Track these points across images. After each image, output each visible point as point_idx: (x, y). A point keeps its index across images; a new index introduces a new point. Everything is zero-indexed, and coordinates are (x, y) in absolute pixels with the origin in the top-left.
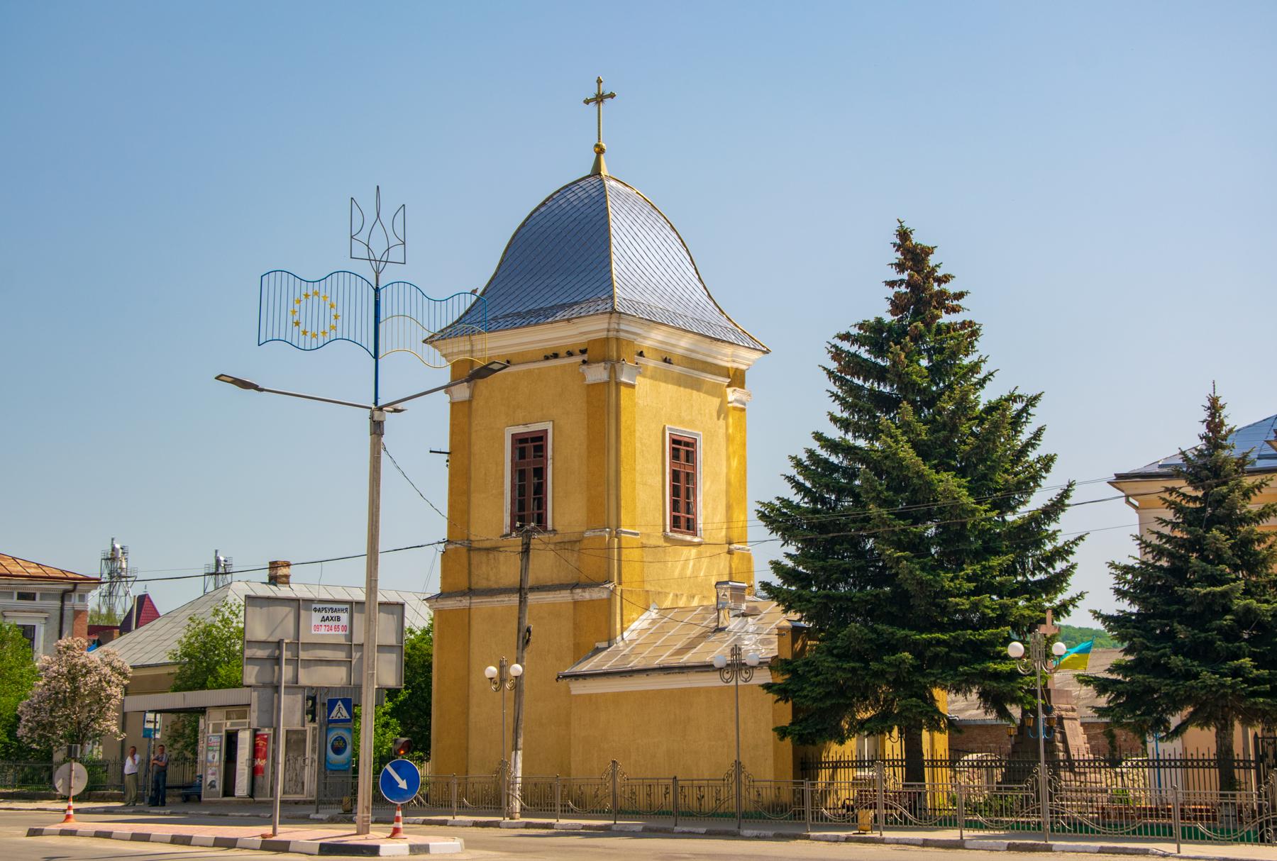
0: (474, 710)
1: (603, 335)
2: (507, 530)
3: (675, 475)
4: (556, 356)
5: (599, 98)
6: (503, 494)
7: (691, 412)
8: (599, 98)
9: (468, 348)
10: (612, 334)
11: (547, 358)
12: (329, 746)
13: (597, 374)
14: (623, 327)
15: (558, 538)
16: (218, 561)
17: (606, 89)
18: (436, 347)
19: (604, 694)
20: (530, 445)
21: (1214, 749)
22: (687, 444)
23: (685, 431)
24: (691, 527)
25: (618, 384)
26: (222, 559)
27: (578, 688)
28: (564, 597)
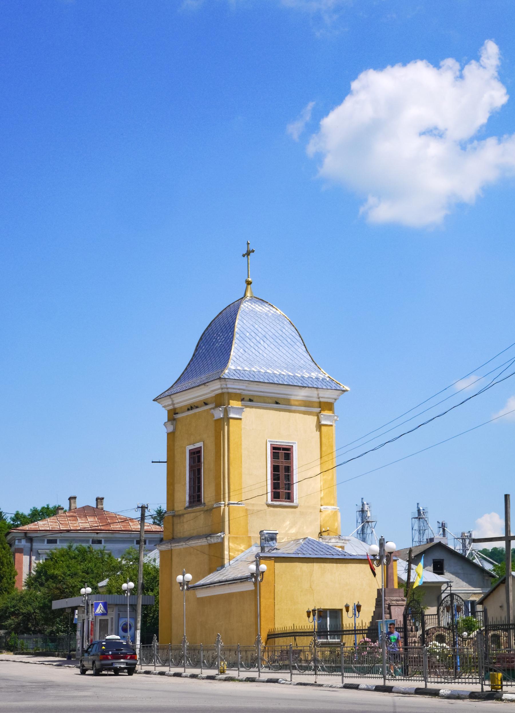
0: (174, 607)
1: (220, 391)
2: (187, 504)
3: (275, 469)
4: (192, 408)
5: (248, 253)
6: (185, 484)
7: (296, 429)
8: (248, 253)
9: (170, 403)
10: (225, 390)
11: (188, 410)
12: (120, 628)
13: (219, 414)
14: (229, 386)
15: (206, 508)
16: (419, 511)
17: (251, 248)
18: (159, 403)
19: (206, 597)
20: (196, 455)
21: (368, 625)
22: (284, 449)
23: (282, 441)
24: (289, 497)
25: (229, 418)
26: (421, 508)
27: (201, 594)
28: (203, 542)
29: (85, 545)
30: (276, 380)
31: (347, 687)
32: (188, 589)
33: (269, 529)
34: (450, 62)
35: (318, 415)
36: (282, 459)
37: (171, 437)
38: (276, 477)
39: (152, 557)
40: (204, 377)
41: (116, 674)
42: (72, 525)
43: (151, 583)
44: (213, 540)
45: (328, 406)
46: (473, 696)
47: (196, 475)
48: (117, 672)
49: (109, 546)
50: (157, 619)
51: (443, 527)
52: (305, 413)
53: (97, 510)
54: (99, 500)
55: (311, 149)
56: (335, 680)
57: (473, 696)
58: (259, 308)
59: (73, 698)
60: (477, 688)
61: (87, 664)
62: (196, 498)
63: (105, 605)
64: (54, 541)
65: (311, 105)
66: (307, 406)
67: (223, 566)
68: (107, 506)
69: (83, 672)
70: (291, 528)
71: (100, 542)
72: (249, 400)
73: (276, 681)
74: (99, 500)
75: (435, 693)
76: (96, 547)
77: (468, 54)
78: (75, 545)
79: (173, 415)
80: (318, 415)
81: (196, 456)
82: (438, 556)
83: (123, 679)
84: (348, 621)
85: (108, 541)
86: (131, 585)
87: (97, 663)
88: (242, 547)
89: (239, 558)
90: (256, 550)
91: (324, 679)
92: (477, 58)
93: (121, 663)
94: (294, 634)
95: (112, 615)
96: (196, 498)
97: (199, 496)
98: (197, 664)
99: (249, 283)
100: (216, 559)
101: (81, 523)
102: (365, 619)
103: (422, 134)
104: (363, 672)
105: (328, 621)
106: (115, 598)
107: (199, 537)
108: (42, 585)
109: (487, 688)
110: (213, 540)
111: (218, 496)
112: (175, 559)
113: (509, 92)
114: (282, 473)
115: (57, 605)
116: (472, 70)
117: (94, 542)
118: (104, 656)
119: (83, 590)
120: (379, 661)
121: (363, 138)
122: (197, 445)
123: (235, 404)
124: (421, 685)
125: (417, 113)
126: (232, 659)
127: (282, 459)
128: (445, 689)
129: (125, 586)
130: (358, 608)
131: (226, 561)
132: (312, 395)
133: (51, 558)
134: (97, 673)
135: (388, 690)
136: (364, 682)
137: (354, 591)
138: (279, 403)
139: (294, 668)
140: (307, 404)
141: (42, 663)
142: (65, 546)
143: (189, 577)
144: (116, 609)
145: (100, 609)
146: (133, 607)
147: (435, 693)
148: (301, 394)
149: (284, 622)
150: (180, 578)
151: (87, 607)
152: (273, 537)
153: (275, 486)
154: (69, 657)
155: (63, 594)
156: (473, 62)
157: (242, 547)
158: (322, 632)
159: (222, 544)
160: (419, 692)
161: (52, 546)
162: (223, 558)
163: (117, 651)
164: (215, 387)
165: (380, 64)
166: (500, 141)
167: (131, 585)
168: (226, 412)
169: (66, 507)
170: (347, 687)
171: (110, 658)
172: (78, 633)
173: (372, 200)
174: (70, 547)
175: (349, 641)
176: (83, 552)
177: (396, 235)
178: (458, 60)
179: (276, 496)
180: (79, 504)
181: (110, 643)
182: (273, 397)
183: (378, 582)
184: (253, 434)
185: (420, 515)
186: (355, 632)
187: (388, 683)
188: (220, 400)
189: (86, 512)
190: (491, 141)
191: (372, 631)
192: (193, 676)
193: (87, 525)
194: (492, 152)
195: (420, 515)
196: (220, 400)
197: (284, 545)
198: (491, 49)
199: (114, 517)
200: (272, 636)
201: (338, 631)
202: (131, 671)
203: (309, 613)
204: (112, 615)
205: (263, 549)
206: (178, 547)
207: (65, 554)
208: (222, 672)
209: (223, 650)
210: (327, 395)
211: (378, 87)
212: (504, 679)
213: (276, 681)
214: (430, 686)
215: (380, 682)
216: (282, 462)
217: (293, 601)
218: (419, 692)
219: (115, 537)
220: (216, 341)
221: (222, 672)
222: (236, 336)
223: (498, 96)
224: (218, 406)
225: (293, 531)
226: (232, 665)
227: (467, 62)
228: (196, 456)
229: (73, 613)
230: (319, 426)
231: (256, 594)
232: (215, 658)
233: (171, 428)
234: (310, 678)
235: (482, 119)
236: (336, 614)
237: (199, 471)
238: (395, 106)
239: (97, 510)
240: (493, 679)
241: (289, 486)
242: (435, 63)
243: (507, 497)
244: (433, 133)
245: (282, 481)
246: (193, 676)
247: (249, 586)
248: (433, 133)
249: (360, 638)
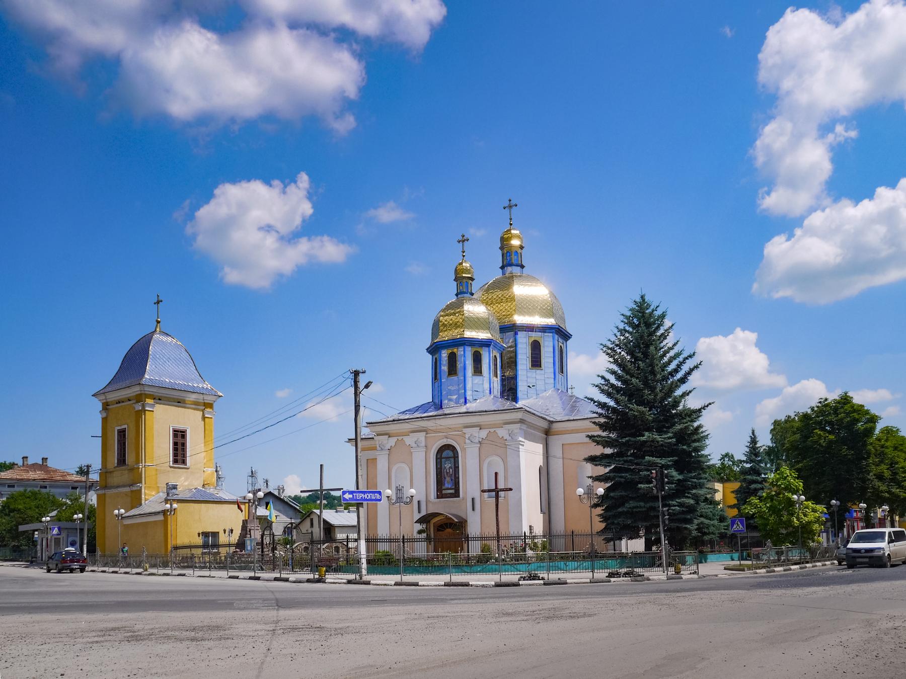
3: (175, 444)
5: (158, 302)
7: (188, 419)
8: (158, 302)
17: (160, 298)
23: (180, 427)
24: (184, 462)
28: (127, 489)
29: (36, 489)
30: (176, 387)
31: (230, 577)
32: (122, 518)
33: (172, 482)
34: (276, 182)
35: (203, 411)
36: (179, 437)
37: (105, 420)
38: (175, 450)
39: (93, 498)
40: (128, 383)
41: (71, 572)
42: (25, 476)
43: (91, 514)
44: (134, 488)
45: (210, 406)
46: (309, 581)
47: (123, 446)
48: (72, 571)
49: (53, 491)
50: (95, 536)
51: (267, 482)
52: (194, 409)
53: (43, 466)
54: (45, 460)
55: (189, 230)
56: (223, 574)
57: (309, 581)
58: (164, 338)
59: (60, 586)
60: (311, 576)
61: (51, 566)
62: (122, 461)
63: (59, 529)
64: (13, 486)
65: (187, 202)
66: (197, 405)
67: (141, 505)
68: (50, 464)
69: (49, 571)
70: (186, 481)
71: (46, 487)
72: (159, 399)
73: (184, 575)
74: (45, 460)
75: (287, 580)
76: (44, 490)
77: (288, 179)
78: (29, 489)
79: (106, 406)
80: (203, 411)
81: (122, 433)
82: (271, 498)
83: (77, 575)
84: (223, 539)
85: (51, 486)
86: (81, 516)
87: (60, 566)
88: (153, 493)
89: (152, 500)
90: (163, 495)
91: (214, 573)
92: (295, 182)
93: (75, 566)
94: (190, 547)
95: (64, 535)
96: (122, 461)
97: (124, 460)
98: (128, 566)
99: (158, 322)
100: (136, 499)
101: (32, 475)
102: (235, 538)
103: (261, 229)
104: (241, 569)
105: (210, 539)
106: (69, 525)
107: (124, 486)
108: (6, 515)
109: (316, 576)
110: (134, 488)
111: (138, 460)
112: (108, 500)
113: (314, 207)
114: (180, 447)
115: (22, 528)
116: (292, 188)
117: (41, 487)
118: (64, 560)
119: (44, 519)
120: (252, 562)
121: (224, 227)
122: (123, 427)
123: (149, 401)
124: (278, 575)
125: (257, 215)
126: (153, 562)
127: (179, 437)
128: (292, 577)
129: (75, 516)
130: (232, 531)
131: (143, 502)
132: (200, 398)
133: (12, 497)
134: (59, 572)
135: (258, 578)
136: (242, 574)
137: (227, 521)
138: (179, 402)
139: (196, 567)
140: (196, 403)
141: (14, 566)
142: (22, 489)
143: (122, 511)
144: (66, 531)
145: (55, 531)
146: (82, 530)
147: (287, 580)
148: (193, 397)
149: (182, 540)
150: (116, 511)
151: (46, 530)
152: (175, 487)
153: (175, 455)
154: (32, 562)
155: (25, 522)
156: (293, 184)
157: (153, 493)
158: (205, 546)
159: (141, 490)
160: (276, 579)
161: (12, 489)
162: (141, 499)
163: (74, 558)
164: (136, 390)
165: (235, 179)
166: (309, 240)
167: (81, 516)
168: (143, 406)
169: (20, 463)
170: (230, 577)
171: (816, 527)
172: (39, 547)
173: (227, 269)
174: (25, 491)
175: (223, 551)
176: (34, 494)
177: (241, 293)
178: (283, 182)
179: (175, 461)
180: (30, 461)
181: (68, 553)
182: (174, 398)
183: (242, 516)
184: (161, 421)
185: (252, 475)
186: (229, 545)
187: (257, 575)
188: (140, 398)
189: (35, 467)
190: (304, 240)
191: (241, 545)
192: (126, 573)
193: (36, 477)
194: (304, 246)
195: (252, 475)
196: (140, 398)
197: (181, 492)
198: (304, 179)
199: (55, 471)
200: (176, 548)
201: (216, 545)
202: (82, 570)
203: (199, 534)
204: (64, 535)
205: (168, 494)
206: (109, 492)
207: (22, 495)
208: (146, 570)
209: (147, 556)
210: (209, 399)
211: (232, 195)
212: (327, 571)
213: (184, 575)
214: (283, 576)
215: (252, 574)
216: (180, 440)
217: (189, 527)
218: (276, 579)
219: (55, 484)
220: (136, 358)
221: (146, 570)
222: (150, 357)
223: (307, 208)
224: (138, 402)
225: (186, 483)
226: (153, 566)
227: (289, 184)
228: (122, 433)
229: (33, 534)
230: (204, 418)
231: (165, 522)
232: (141, 562)
233: (105, 415)
234: (206, 573)
235: (298, 221)
236: (215, 535)
237: (124, 444)
238: (243, 207)
239: (43, 466)
240: (320, 572)
241: (184, 456)
242: (268, 182)
243: (321, 465)
244: (268, 229)
245: (180, 452)
246: (126, 573)
247: (160, 518)
248: (268, 229)
249: (233, 549)
